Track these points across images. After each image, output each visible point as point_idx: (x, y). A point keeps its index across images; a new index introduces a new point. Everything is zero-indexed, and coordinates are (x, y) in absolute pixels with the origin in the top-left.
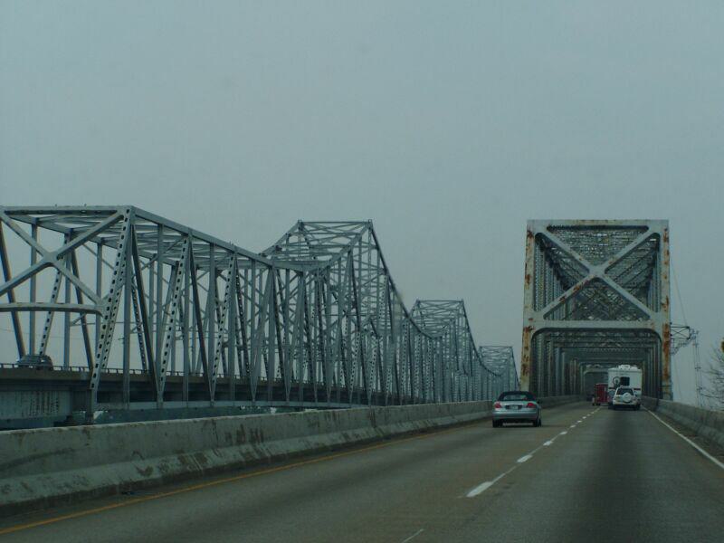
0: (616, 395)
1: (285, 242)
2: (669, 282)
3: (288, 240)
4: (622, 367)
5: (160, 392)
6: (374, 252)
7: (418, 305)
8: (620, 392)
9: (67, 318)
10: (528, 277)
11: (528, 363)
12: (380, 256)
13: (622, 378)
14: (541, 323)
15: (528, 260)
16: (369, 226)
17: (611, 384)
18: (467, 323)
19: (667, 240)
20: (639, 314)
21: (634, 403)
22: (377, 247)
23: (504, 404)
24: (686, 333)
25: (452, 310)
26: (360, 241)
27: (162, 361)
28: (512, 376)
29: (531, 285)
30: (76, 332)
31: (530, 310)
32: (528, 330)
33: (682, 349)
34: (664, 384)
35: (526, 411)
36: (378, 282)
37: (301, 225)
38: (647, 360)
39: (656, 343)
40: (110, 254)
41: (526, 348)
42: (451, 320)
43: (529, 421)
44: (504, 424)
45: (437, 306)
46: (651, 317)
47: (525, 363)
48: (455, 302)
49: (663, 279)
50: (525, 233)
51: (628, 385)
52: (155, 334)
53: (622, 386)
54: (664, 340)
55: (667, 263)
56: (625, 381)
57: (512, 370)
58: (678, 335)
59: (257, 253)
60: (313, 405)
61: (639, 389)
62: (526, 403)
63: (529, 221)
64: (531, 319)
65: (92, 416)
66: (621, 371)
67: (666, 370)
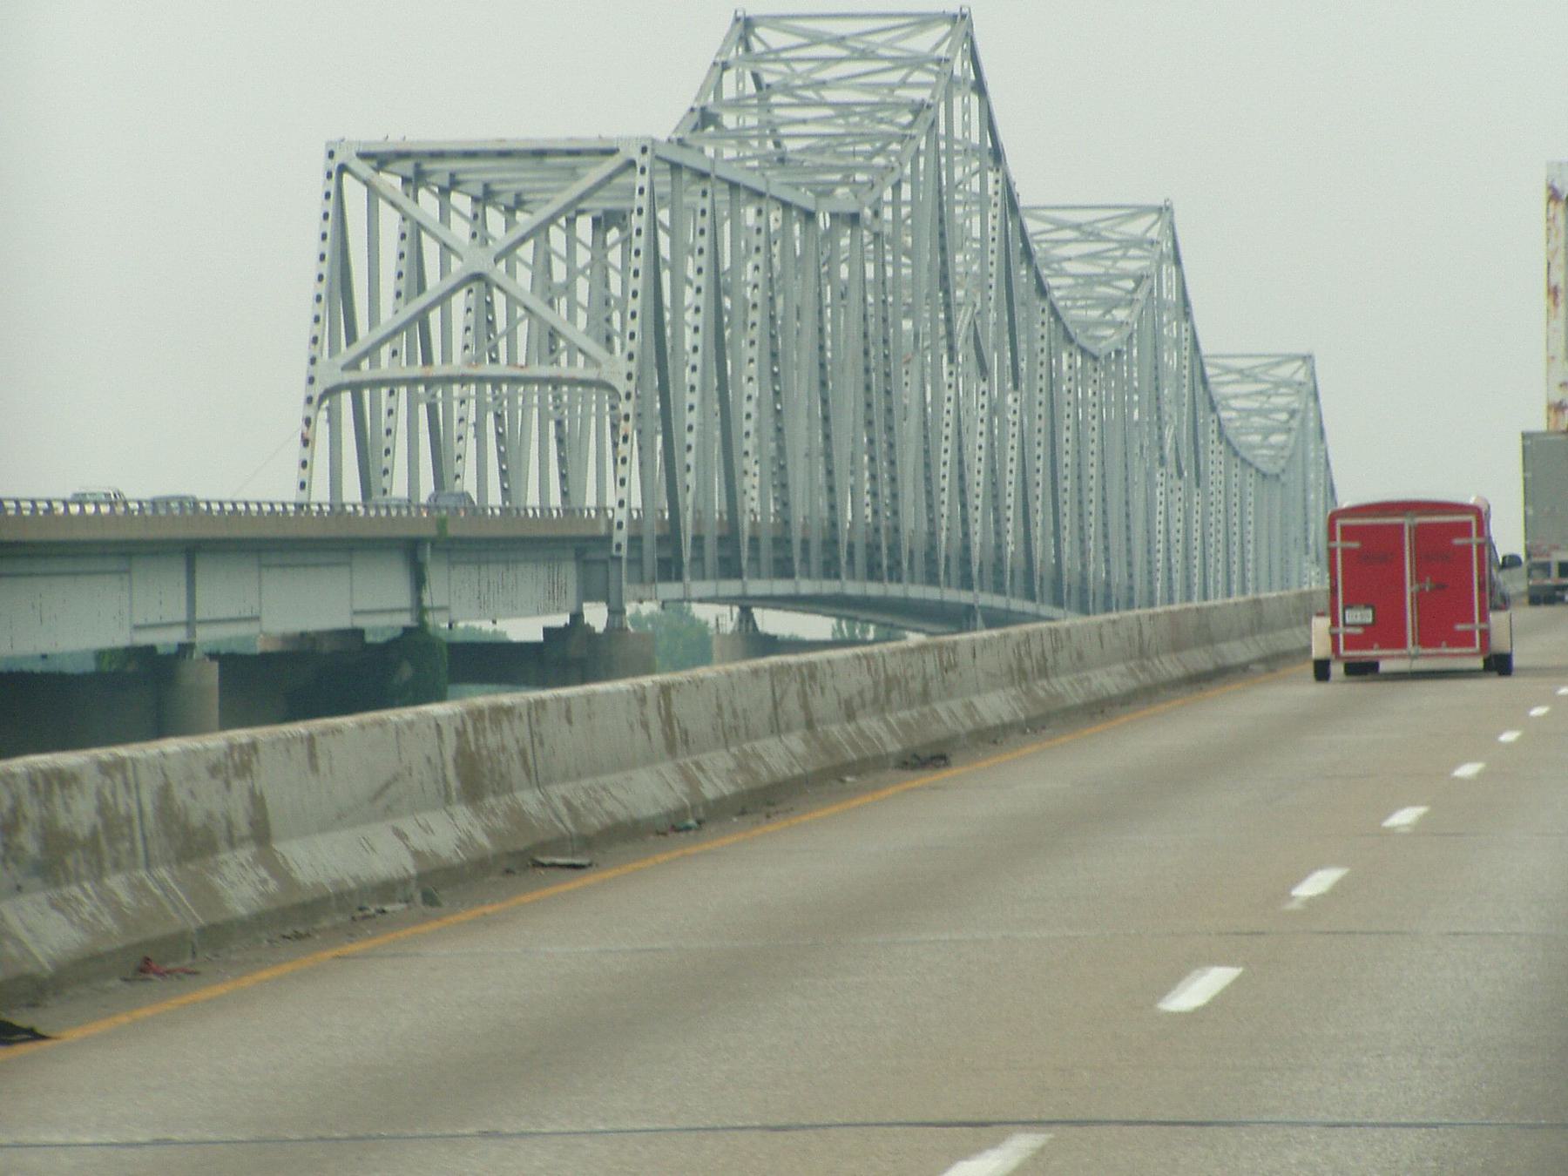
7: (744, 41)
15: (1552, 254)
18: (990, 125)
28: (1170, 359)
42: (918, 109)
45: (840, 41)
48: (924, 21)
50: (1543, 194)
57: (1171, 330)
65: (623, 611)
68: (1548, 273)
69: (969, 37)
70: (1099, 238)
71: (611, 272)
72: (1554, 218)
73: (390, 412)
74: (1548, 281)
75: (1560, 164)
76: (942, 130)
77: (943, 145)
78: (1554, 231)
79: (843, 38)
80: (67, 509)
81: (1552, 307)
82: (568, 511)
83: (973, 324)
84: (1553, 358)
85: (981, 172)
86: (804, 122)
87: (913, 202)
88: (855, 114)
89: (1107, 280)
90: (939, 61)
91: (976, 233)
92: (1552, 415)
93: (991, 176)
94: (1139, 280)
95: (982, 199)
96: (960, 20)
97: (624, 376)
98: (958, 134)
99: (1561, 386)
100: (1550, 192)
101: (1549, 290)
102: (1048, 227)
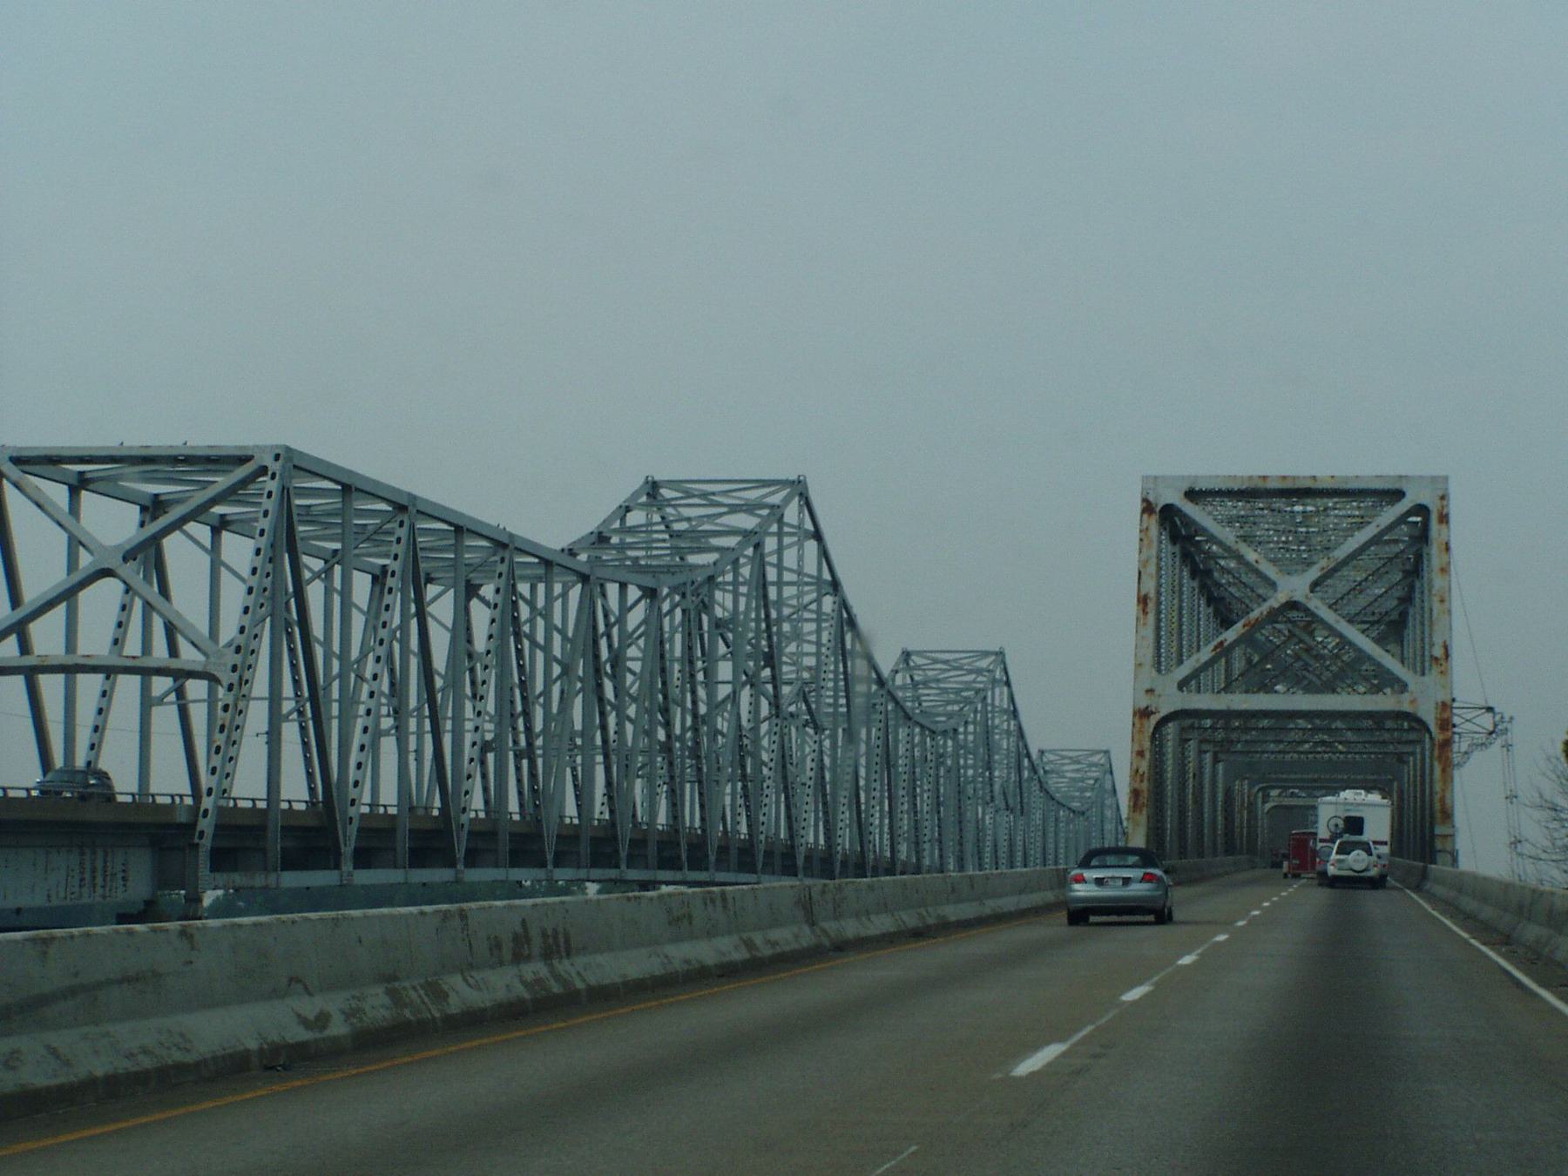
0: (1334, 856)
2: (1449, 611)
3: (623, 519)
4: (1347, 795)
6: (811, 546)
8: (1345, 849)
9: (145, 689)
10: (1143, 600)
11: (1145, 786)
12: (824, 554)
13: (1348, 820)
14: (1171, 700)
15: (1144, 564)
16: (799, 489)
18: (1012, 699)
19: (1444, 519)
20: (1383, 680)
21: (1374, 872)
22: (817, 535)
23: (1090, 874)
24: (1487, 721)
25: (979, 671)
26: (780, 521)
28: (1108, 813)
29: (1151, 618)
30: (165, 719)
31: (1149, 671)
32: (1143, 714)
33: (1477, 756)
34: (1438, 830)
35: (1139, 889)
36: (819, 612)
39: (1420, 742)
40: (239, 551)
41: (1141, 754)
44: (1093, 919)
45: (946, 662)
46: (1411, 687)
47: (1137, 785)
48: (986, 654)
49: (1436, 606)
50: (1138, 506)
51: (1361, 833)
52: (335, 723)
53: (1347, 837)
54: (1439, 736)
55: (1445, 570)
58: (1469, 725)
59: (558, 548)
60: (678, 876)
61: (1385, 843)
63: (1145, 479)
64: (1150, 691)
65: (200, 900)
66: (1346, 803)
67: (1443, 800)
68: (1139, 583)
69: (1004, 663)
70: (1079, 763)
71: (354, 612)
72: (1147, 529)
73: (359, 766)
75: (1156, 478)
76: (989, 701)
77: (989, 708)
78: (1145, 542)
79: (948, 661)
81: (1142, 616)
83: (1002, 786)
84: (1140, 665)
85: (1008, 720)
86: (928, 695)
87: (974, 733)
89: (1082, 780)
90: (989, 671)
91: (1005, 747)
92: (1137, 720)
93: (1012, 723)
94: (1096, 780)
95: (1008, 732)
96: (1000, 654)
97: (229, 667)
98: (997, 703)
100: (1145, 505)
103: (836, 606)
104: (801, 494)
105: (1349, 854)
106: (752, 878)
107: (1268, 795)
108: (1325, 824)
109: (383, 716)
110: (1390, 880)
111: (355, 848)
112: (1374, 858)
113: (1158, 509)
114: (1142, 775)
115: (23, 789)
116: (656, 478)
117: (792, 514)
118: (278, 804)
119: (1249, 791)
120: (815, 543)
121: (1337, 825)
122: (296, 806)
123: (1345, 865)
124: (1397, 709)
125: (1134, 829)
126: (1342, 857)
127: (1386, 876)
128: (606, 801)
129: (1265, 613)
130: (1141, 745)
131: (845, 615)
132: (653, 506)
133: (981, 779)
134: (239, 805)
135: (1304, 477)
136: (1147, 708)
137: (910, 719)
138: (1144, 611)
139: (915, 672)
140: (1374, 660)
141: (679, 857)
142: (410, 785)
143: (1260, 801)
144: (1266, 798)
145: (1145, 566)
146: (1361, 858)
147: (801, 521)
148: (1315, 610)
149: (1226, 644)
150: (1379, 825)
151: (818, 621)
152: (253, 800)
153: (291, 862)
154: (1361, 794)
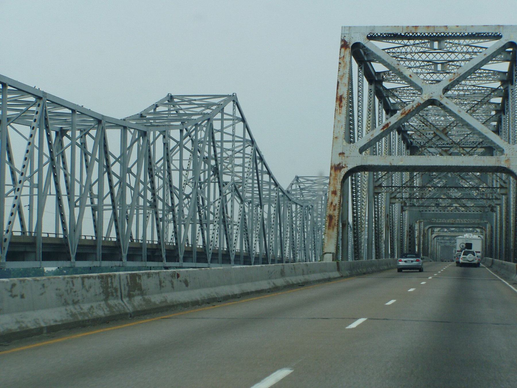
0: (462, 256)
1: (152, 111)
3: (155, 109)
4: (467, 235)
5: (181, 256)
6: (240, 125)
10: (340, 99)
12: (246, 127)
13: (467, 244)
15: (341, 77)
16: (234, 99)
17: (458, 249)
21: (476, 261)
22: (243, 120)
23: (403, 260)
26: (222, 111)
27: (197, 236)
29: (344, 109)
31: (342, 143)
32: (337, 168)
35: (415, 263)
36: (244, 153)
37: (171, 98)
38: (491, 221)
43: (418, 269)
44: (403, 271)
45: (312, 181)
46: (506, 152)
50: (339, 44)
51: (471, 248)
53: (466, 250)
56: (469, 246)
60: (160, 264)
61: (479, 252)
62: (415, 259)
63: (344, 28)
64: (342, 154)
66: (466, 238)
68: (338, 88)
72: (344, 57)
74: (337, 93)
75: (350, 27)
78: (342, 65)
80: (169, 244)
81: (338, 108)
82: (23, 232)
84: (336, 138)
88: (311, 192)
92: (333, 172)
99: (340, 154)
100: (343, 43)
101: (337, 98)
102: (306, 180)
103: (253, 151)
104: (234, 101)
105: (467, 255)
106: (206, 265)
107: (434, 231)
108: (459, 245)
109: (48, 195)
110: (481, 265)
111: (127, 254)
112: (476, 256)
113: (351, 46)
114: (335, 206)
115: (46, 233)
116: (298, 176)
117: (229, 108)
118: (41, 235)
119: (424, 228)
120: (243, 123)
121: (463, 246)
122: (50, 236)
123: (465, 259)
124: (497, 165)
125: (328, 241)
126: (464, 256)
127: (480, 263)
128: (173, 234)
129: (415, 106)
130: (335, 187)
131: (258, 155)
132: (171, 105)
133: (324, 226)
134: (50, 236)
135: (440, 27)
136: (340, 164)
137: (290, 200)
138: (340, 105)
139: (300, 184)
140: (482, 135)
141: (161, 256)
142: (125, 230)
143: (430, 234)
144: (433, 232)
145: (341, 79)
146: (471, 256)
147: (234, 113)
148: (446, 105)
149: (390, 125)
150: (477, 247)
151: (244, 158)
152: (48, 234)
153: (105, 258)
154: (471, 235)
